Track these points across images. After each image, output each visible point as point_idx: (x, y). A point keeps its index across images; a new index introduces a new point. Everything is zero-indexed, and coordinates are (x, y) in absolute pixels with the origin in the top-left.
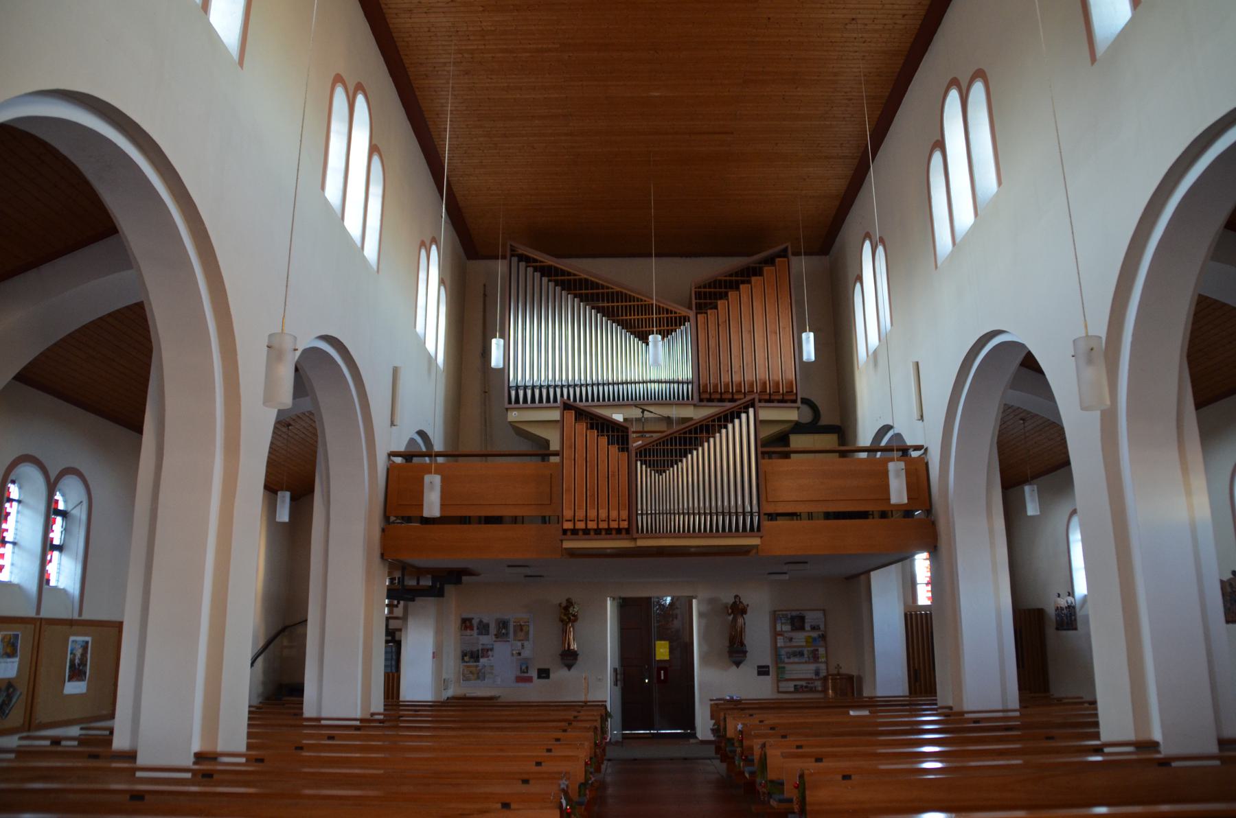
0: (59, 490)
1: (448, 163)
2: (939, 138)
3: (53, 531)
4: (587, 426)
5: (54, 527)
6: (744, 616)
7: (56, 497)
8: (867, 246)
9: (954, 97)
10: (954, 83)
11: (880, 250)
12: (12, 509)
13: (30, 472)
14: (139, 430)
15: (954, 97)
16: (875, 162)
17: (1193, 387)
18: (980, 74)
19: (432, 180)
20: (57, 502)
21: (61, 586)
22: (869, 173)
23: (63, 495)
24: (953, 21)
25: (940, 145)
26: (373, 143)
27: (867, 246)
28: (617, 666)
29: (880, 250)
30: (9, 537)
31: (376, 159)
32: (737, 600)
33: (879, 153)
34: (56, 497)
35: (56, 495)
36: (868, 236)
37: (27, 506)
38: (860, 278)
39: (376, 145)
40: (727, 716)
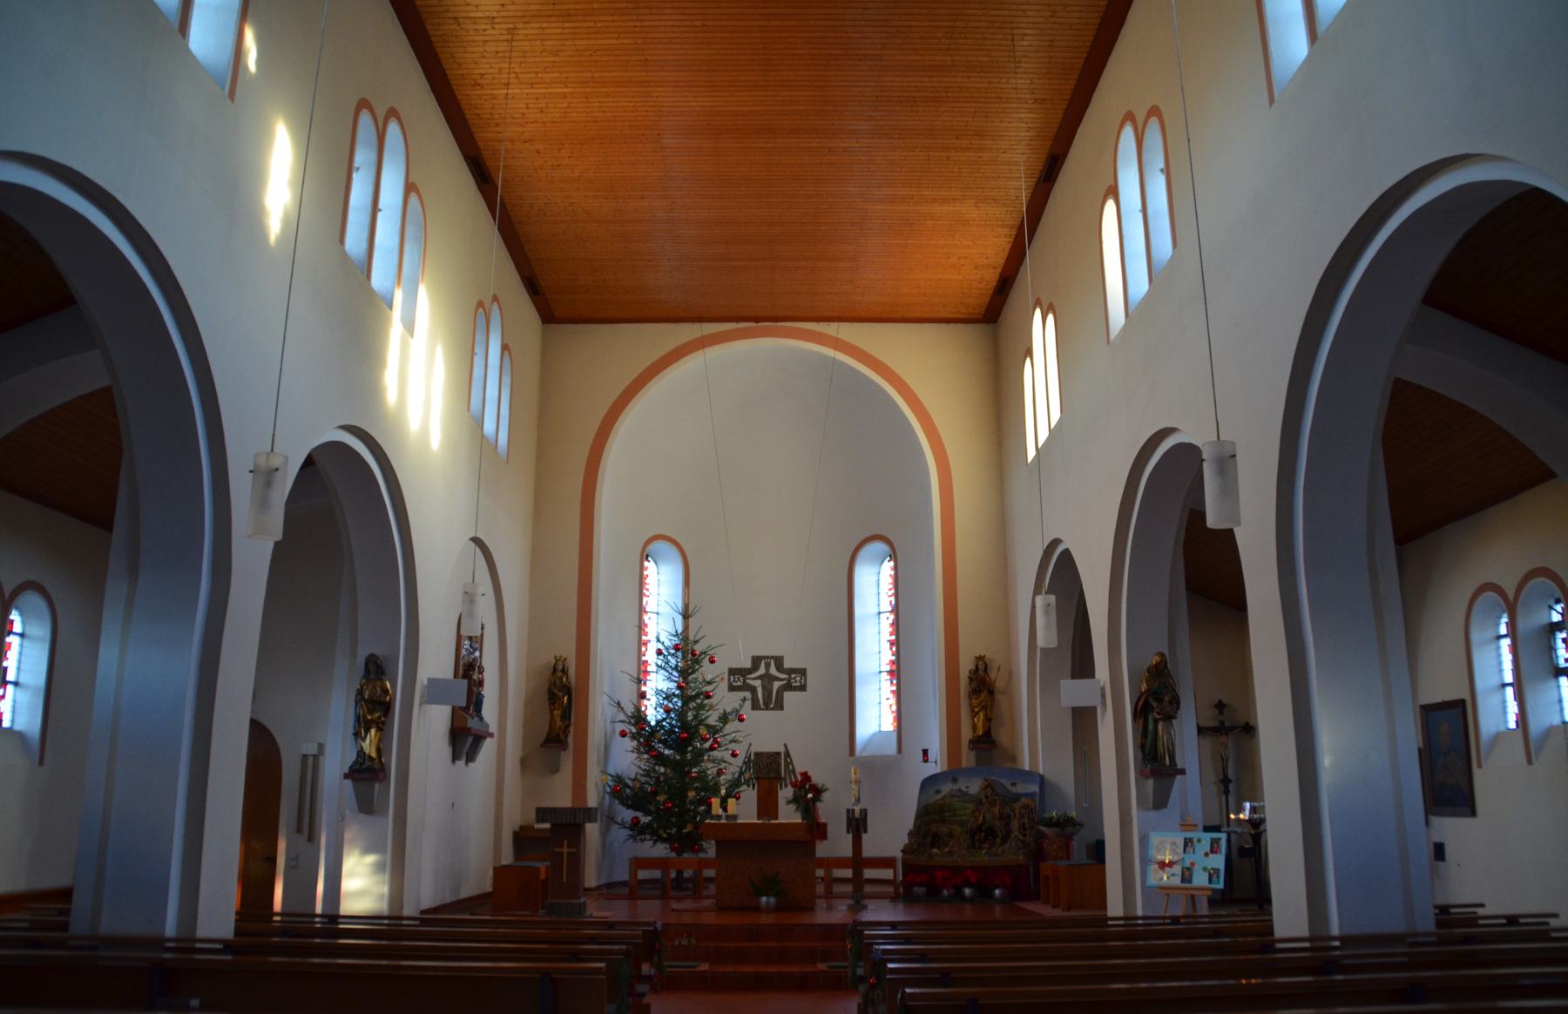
0: (17, 608)
1: (502, 185)
2: (1113, 184)
3: (7, 659)
4: (789, 763)
5: (9, 654)
6: (631, 840)
7: (12, 617)
8: (1038, 312)
9: (1128, 136)
10: (1129, 117)
11: (1050, 318)
12: (13, 640)
13: (33, 600)
14: (108, 526)
15: (1128, 136)
16: (1033, 243)
17: (1386, 463)
18: (1155, 111)
19: (458, 150)
20: (12, 622)
21: (17, 727)
22: (1025, 261)
23: (21, 614)
24: (1136, 19)
25: (1113, 192)
26: (410, 181)
27: (1038, 312)
28: (1421, 746)
29: (1050, 318)
30: (11, 676)
31: (413, 199)
32: (981, 667)
33: (1034, 241)
34: (12, 617)
35: (11, 613)
36: (1038, 303)
37: (31, 638)
38: (1029, 352)
39: (413, 184)
40: (617, 720)
